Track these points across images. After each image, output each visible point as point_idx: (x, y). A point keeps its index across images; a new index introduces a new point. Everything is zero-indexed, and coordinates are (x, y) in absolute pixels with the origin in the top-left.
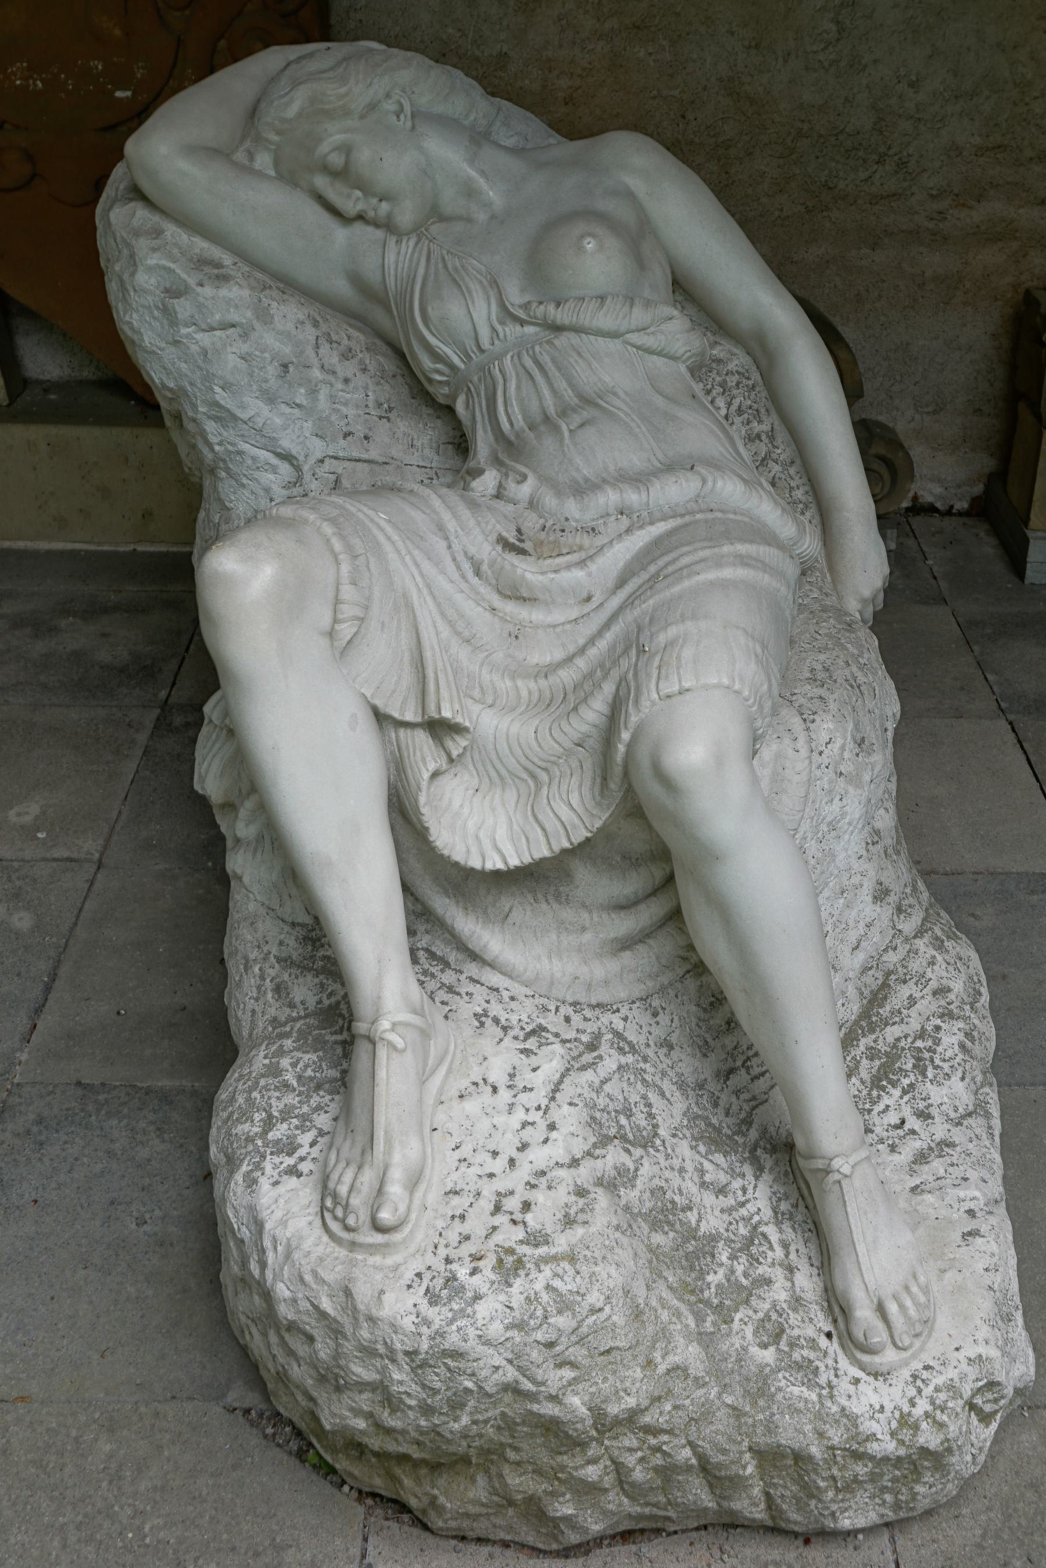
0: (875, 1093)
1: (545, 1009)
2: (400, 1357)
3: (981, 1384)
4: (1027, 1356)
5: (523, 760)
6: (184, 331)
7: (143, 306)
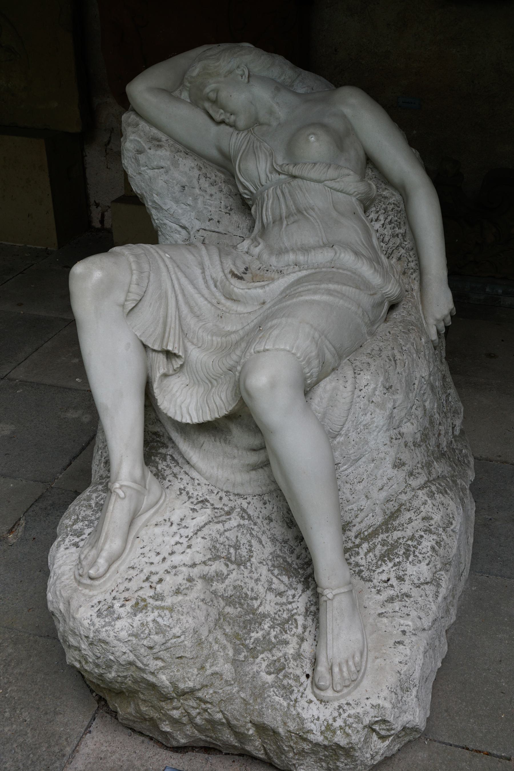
0: (380, 563)
1: (212, 492)
2: (83, 638)
3: (377, 719)
4: (415, 711)
5: (206, 374)
6: (142, 169)
7: (128, 157)
